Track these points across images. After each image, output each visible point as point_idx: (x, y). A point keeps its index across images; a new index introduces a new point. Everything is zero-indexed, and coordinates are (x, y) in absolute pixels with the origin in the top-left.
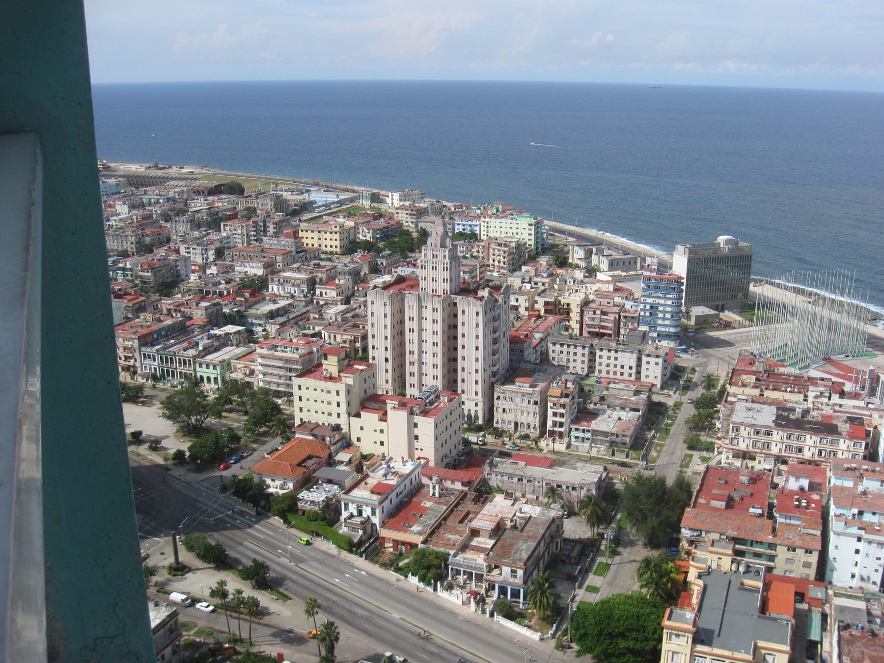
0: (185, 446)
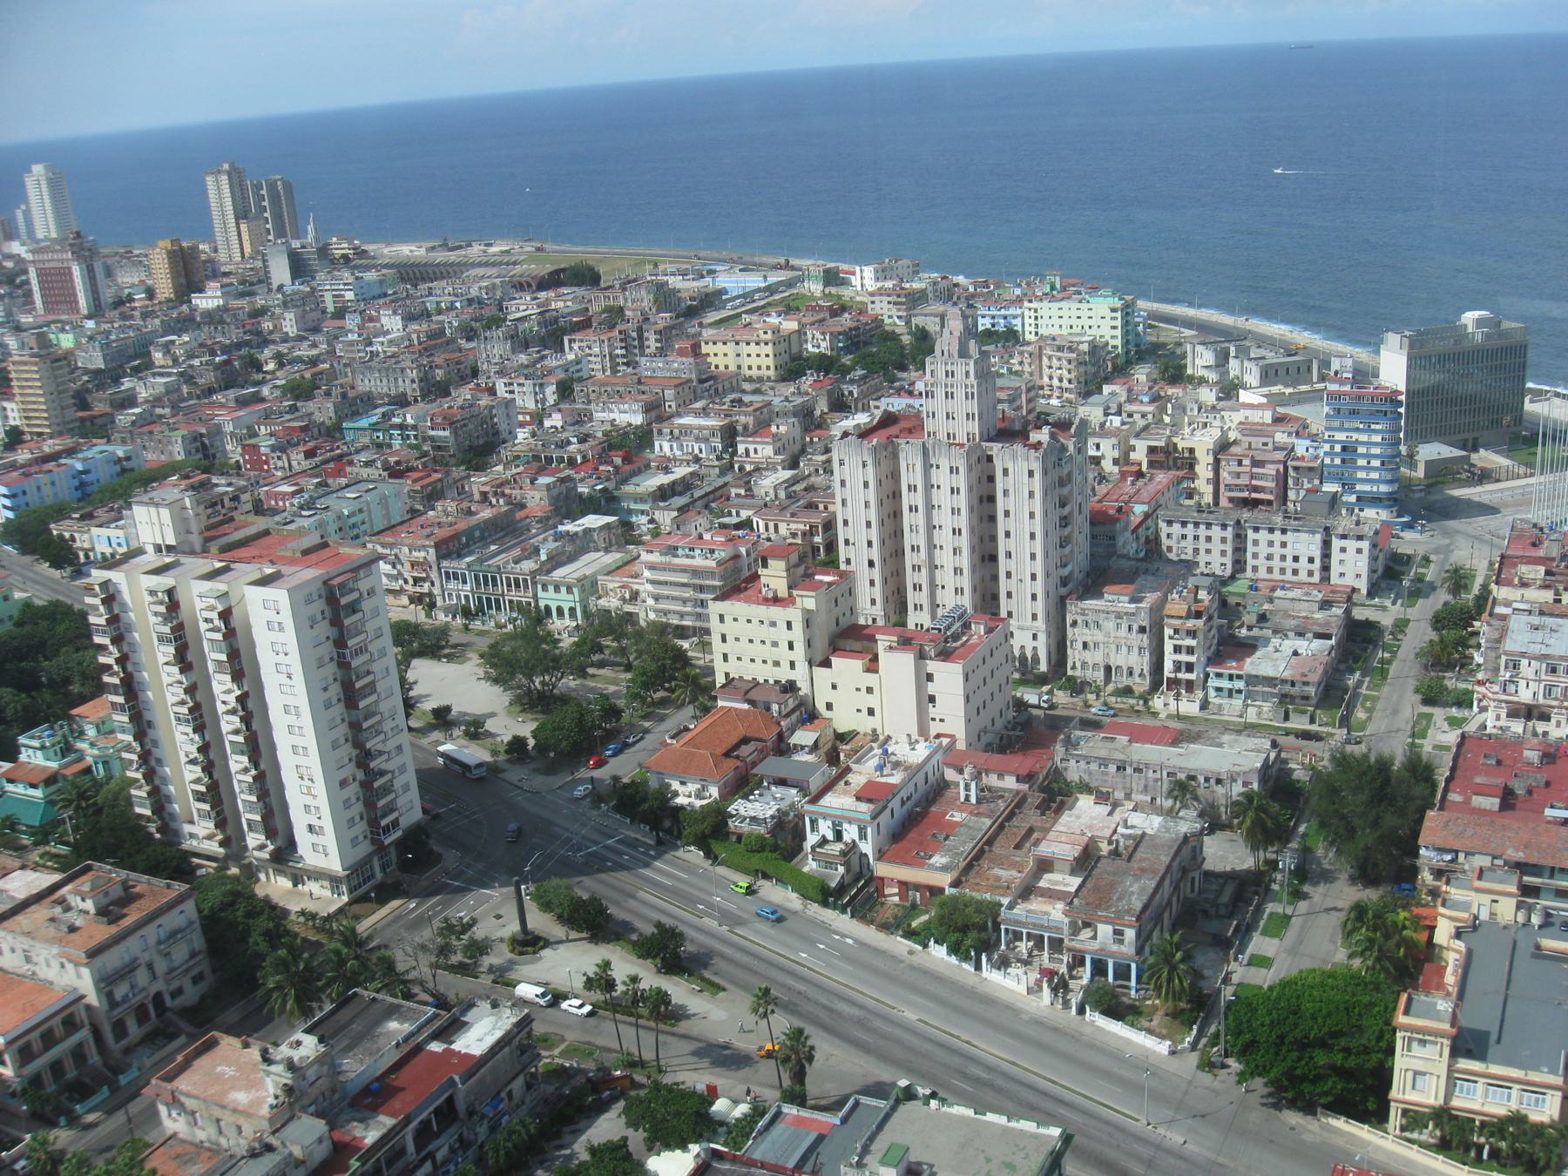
0: (526, 728)
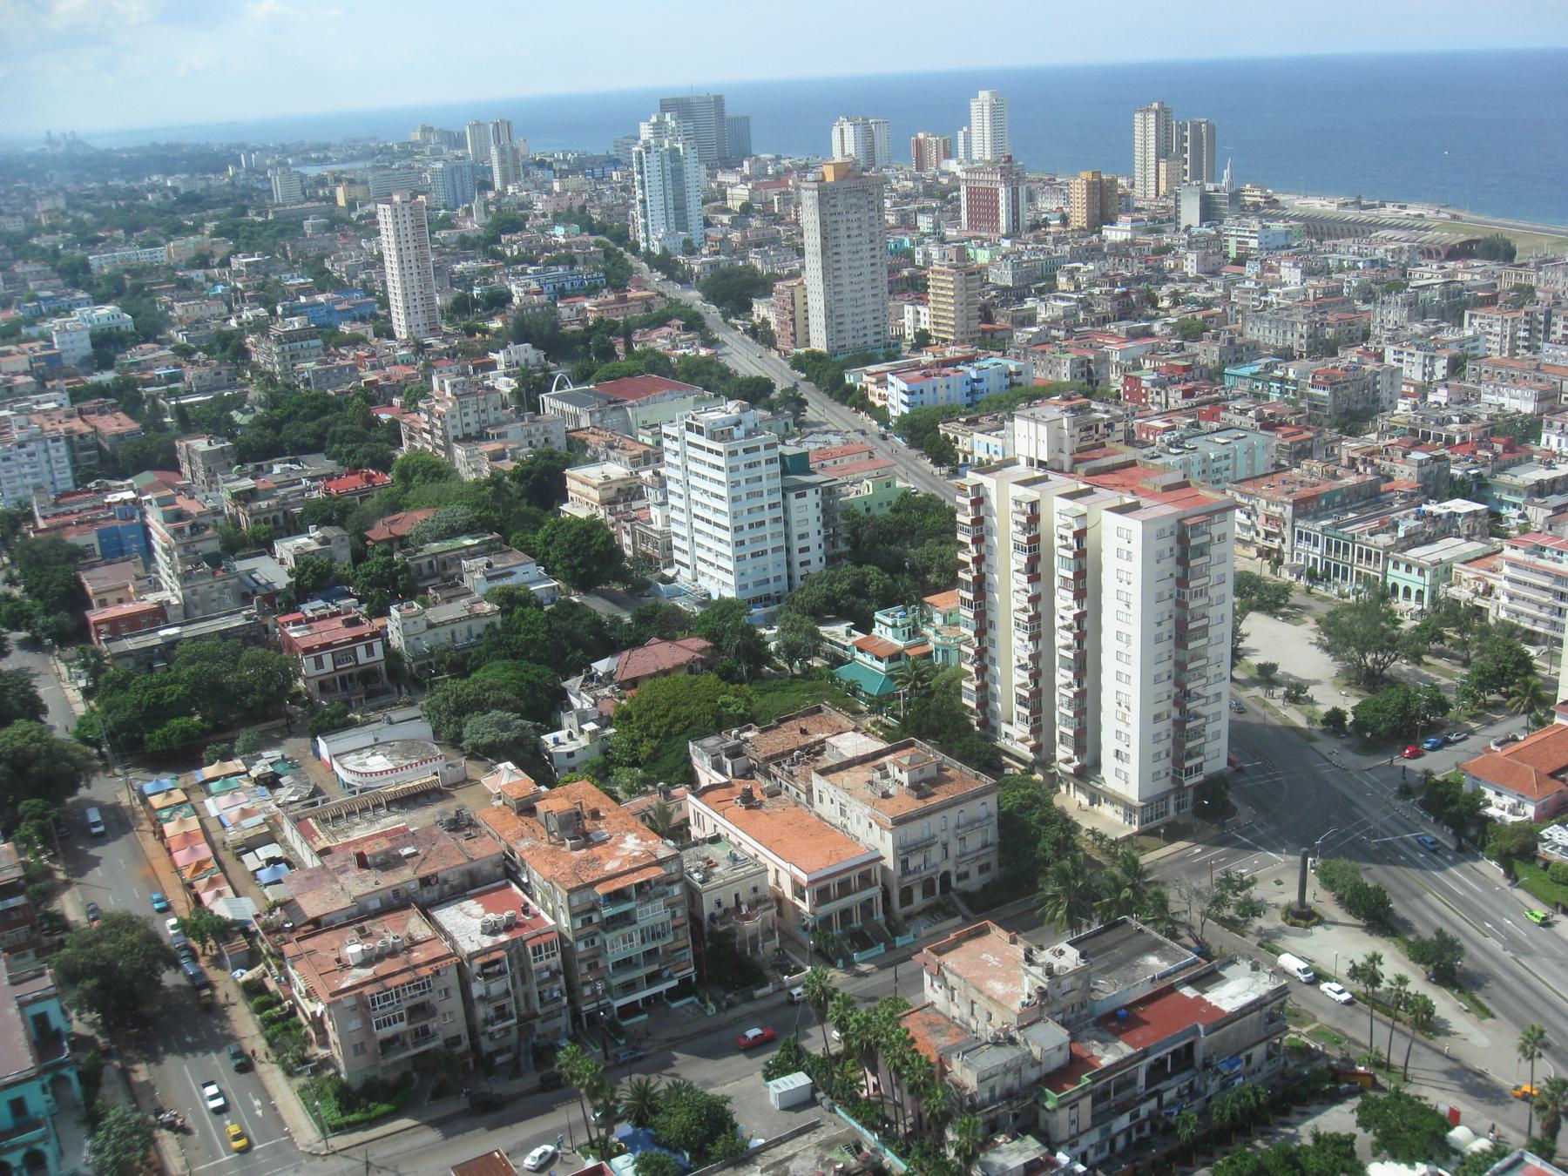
0: (1347, 703)
